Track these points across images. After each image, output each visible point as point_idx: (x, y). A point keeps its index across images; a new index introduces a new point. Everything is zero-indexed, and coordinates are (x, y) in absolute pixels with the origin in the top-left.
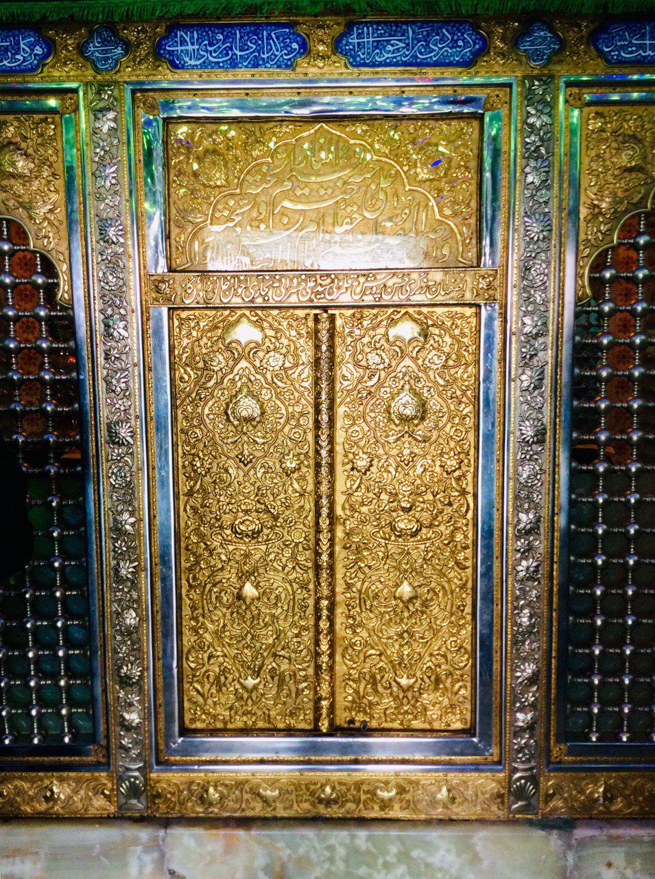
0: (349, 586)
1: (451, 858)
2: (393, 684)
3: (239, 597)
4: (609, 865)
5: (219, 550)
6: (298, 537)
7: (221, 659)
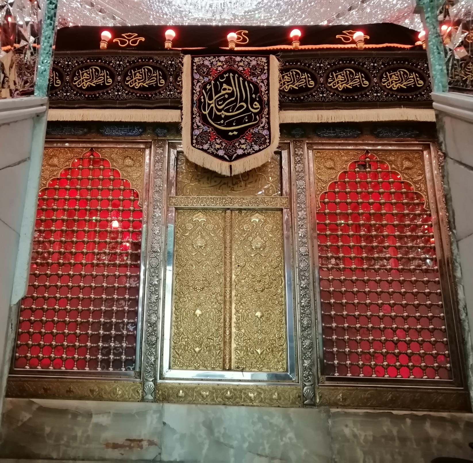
0: (237, 311)
1: (280, 420)
2: (255, 352)
3: (194, 314)
4: (346, 426)
5: (188, 295)
6: (218, 289)
7: (186, 339)
